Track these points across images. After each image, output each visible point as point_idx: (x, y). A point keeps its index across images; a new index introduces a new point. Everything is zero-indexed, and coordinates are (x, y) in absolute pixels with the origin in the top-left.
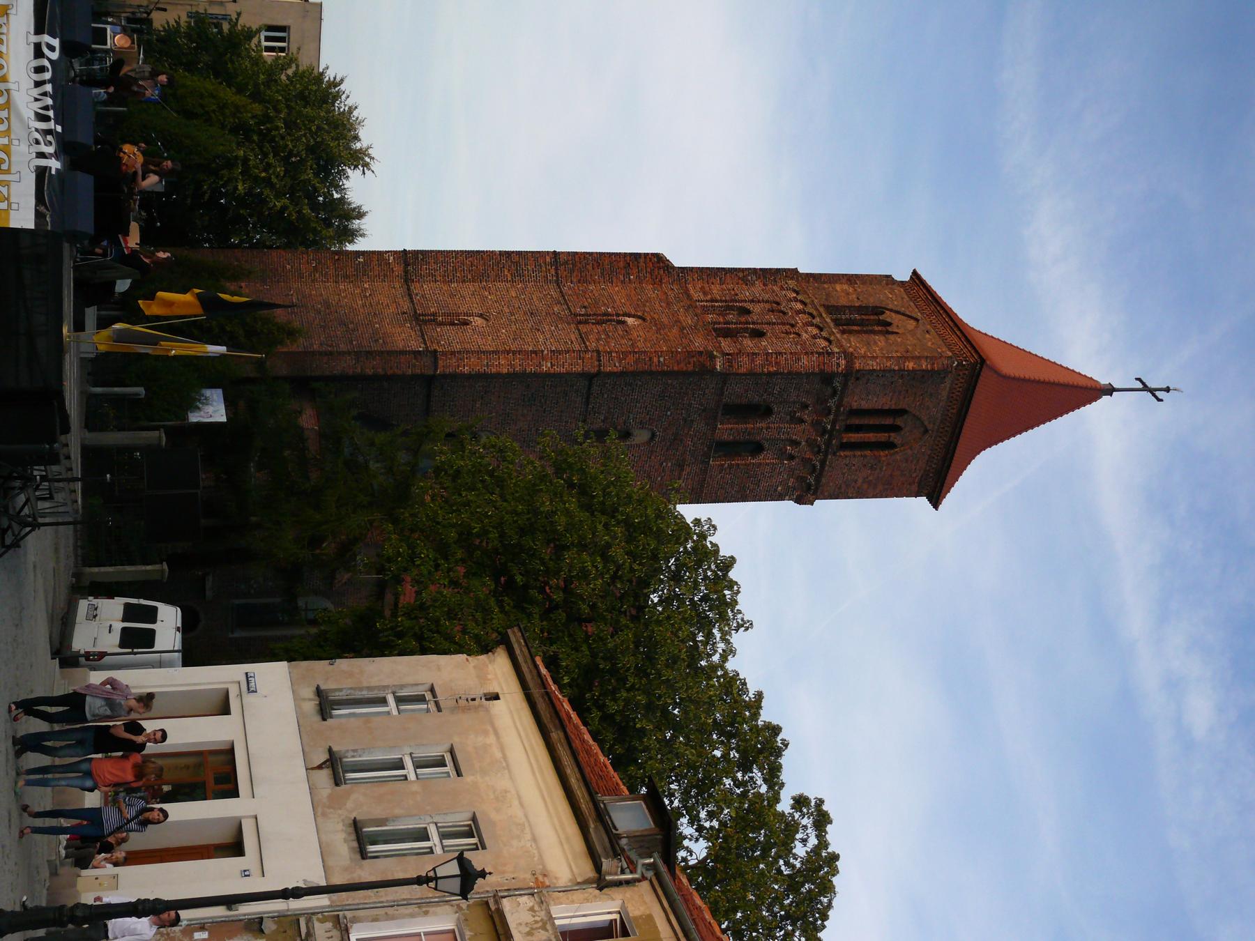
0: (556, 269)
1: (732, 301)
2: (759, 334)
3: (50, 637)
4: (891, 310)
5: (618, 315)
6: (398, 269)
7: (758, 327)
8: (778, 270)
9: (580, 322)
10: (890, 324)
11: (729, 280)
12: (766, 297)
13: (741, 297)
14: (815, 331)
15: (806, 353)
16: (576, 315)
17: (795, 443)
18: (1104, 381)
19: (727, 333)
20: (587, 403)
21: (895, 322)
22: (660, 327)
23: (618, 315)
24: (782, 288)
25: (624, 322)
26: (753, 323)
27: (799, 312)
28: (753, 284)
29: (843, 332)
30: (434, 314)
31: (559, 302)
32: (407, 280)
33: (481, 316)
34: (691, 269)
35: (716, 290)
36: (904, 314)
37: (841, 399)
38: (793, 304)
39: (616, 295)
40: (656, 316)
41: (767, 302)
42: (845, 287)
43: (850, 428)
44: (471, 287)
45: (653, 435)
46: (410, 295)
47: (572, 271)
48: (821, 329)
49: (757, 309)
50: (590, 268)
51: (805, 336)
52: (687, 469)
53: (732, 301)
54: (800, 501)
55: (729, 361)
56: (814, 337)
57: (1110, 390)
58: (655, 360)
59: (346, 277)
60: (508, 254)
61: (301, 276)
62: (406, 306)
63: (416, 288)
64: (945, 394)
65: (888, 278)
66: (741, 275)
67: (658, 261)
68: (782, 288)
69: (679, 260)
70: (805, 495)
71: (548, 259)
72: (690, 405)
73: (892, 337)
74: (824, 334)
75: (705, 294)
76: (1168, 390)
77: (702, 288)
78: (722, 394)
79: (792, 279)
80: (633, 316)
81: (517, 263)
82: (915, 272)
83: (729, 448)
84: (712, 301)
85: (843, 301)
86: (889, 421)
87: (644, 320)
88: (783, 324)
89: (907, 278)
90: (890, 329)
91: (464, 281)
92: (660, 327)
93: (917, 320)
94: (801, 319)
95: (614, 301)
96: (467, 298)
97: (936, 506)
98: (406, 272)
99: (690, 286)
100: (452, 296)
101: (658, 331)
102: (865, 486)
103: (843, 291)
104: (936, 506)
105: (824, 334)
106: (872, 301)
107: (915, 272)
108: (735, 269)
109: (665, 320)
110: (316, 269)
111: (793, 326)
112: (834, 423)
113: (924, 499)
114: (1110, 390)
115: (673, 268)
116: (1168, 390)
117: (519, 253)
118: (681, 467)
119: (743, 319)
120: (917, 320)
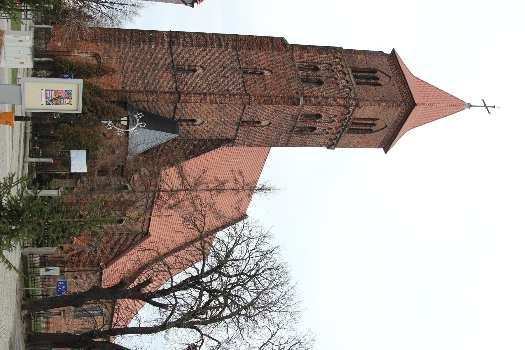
0: (236, 43)
1: (312, 63)
2: (320, 83)
3: (48, 77)
4: (380, 71)
5: (261, 69)
6: (167, 40)
7: (321, 78)
8: (334, 47)
9: (244, 73)
10: (378, 79)
11: (311, 51)
12: (327, 61)
13: (315, 61)
14: (345, 83)
15: (339, 98)
16: (243, 68)
17: (330, 129)
18: (467, 102)
19: (306, 81)
20: (243, 111)
21: (381, 78)
22: (279, 78)
23: (261, 69)
24: (334, 57)
25: (262, 74)
26: (319, 77)
27: (340, 71)
28: (322, 53)
29: (357, 83)
30: (181, 65)
31: (236, 61)
32: (171, 44)
33: (202, 67)
34: (296, 45)
35: (305, 56)
36: (385, 74)
37: (351, 115)
38: (338, 66)
39: (261, 58)
40: (277, 71)
41: (327, 64)
42: (362, 56)
43: (354, 124)
44: (199, 50)
45: (270, 124)
46: (171, 54)
47: (243, 44)
48: (348, 82)
49: (321, 67)
50: (251, 42)
51: (340, 85)
52: (283, 135)
53: (312, 63)
54: (329, 148)
55: (306, 100)
56: (344, 86)
57: (470, 106)
58: (274, 100)
59: (144, 42)
60: (216, 35)
61: (125, 41)
62: (169, 60)
63: (174, 49)
65: (382, 53)
66: (317, 49)
67: (281, 41)
68: (334, 57)
69: (291, 41)
70: (331, 146)
71: (233, 38)
72: (287, 114)
73: (378, 87)
74: (349, 85)
75: (300, 58)
76: (494, 107)
77: (300, 54)
78: (301, 110)
79: (339, 52)
80: (268, 70)
81: (220, 39)
82: (393, 51)
83: (302, 130)
84: (303, 62)
85: (359, 65)
86: (371, 122)
87: (272, 73)
88: (332, 77)
89: (390, 53)
90: (378, 82)
91: (196, 47)
92: (279, 78)
93: (390, 78)
94: (340, 75)
95: (260, 61)
96: (196, 57)
97: (386, 152)
98: (170, 41)
99: (294, 53)
100: (190, 54)
101: (278, 79)
102: (357, 144)
104: (386, 152)
105: (349, 85)
106: (372, 66)
107: (393, 51)
108: (315, 46)
109: (281, 73)
110: (131, 38)
111: (336, 79)
112: (347, 123)
113: (390, 53)
114: (470, 106)
115: (288, 44)
117: (221, 35)
118: (280, 134)
119: (315, 74)
120: (390, 78)
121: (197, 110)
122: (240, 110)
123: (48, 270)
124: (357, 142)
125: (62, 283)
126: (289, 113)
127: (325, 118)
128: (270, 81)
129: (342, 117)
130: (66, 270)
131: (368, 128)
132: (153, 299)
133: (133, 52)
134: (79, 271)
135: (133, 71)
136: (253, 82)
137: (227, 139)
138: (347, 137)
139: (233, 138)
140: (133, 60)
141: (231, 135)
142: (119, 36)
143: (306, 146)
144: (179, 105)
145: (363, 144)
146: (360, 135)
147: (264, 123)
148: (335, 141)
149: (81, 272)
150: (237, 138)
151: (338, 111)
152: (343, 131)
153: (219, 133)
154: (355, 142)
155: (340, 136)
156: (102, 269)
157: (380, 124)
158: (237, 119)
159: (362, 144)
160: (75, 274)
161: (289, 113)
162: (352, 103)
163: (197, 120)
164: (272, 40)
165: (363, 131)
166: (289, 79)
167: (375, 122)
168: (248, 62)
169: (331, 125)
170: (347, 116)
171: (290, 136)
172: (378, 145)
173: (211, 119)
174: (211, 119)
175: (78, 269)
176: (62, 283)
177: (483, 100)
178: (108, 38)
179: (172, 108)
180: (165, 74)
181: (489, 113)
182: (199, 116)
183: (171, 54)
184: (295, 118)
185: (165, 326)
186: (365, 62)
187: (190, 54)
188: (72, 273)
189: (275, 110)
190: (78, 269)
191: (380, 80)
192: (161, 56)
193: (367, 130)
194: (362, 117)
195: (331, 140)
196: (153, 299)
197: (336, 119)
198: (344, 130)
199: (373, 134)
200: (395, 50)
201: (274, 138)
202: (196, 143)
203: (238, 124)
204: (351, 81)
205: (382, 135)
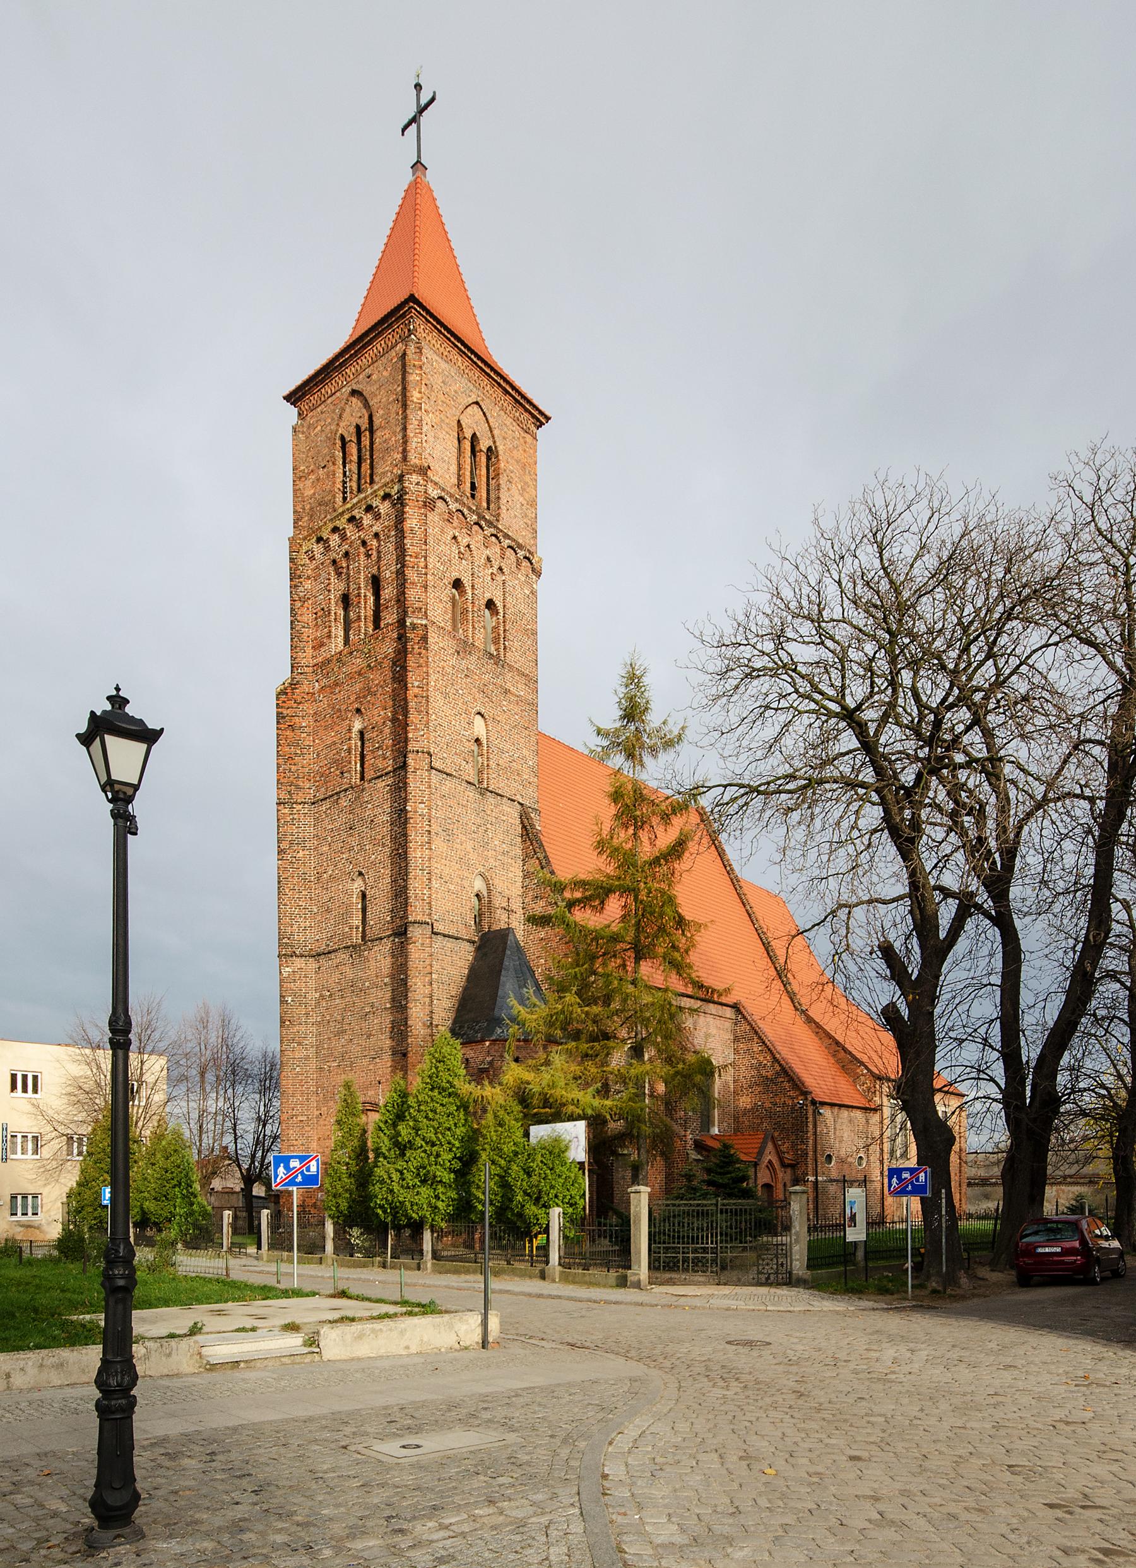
18: (408, 177)
40: (353, 698)
46: (329, 953)
47: (298, 787)
50: (293, 768)
52: (509, 686)
62: (342, 956)
64: (444, 365)
76: (418, 87)
82: (287, 398)
86: (467, 445)
89: (294, 411)
95: (334, 743)
100: (328, 911)
102: (527, 496)
103: (313, 485)
107: (287, 398)
108: (292, 610)
109: (357, 687)
110: (299, 1044)
116: (418, 87)
121: (452, 887)
122: (449, 783)
123: (853, 1217)
124: (522, 495)
125: (895, 1180)
126: (453, 662)
127: (460, 569)
128: (376, 712)
129: (456, 522)
130: (811, 1178)
131: (484, 459)
132: (942, 935)
133: (329, 1039)
134: (815, 1151)
135: (368, 1037)
136: (380, 752)
137: (524, 827)
138: (511, 520)
139: (519, 807)
140: (346, 1037)
141: (512, 814)
142: (298, 1069)
143: (535, 633)
144: (439, 927)
145: (527, 478)
146: (503, 480)
147: (479, 728)
148: (521, 553)
149: (819, 1147)
150: (519, 798)
151: (442, 531)
152: (495, 527)
153: (507, 840)
154: (521, 499)
155: (506, 536)
156: (814, 1102)
157: (473, 422)
158: (471, 794)
159: (526, 483)
160: (821, 1159)
161: (453, 661)
162: (417, 484)
163: (476, 890)
164: (284, 717)
165: (493, 475)
166: (369, 666)
167: (468, 435)
168: (338, 772)
169: (480, 554)
170: (454, 506)
171: (510, 666)
172: (528, 438)
173: (473, 856)
174: (473, 856)
175: (811, 1153)
176: (895, 1180)
177: (404, 130)
178: (302, 1095)
179: (449, 944)
180: (372, 963)
181: (433, 100)
182: (466, 883)
183: (329, 953)
184: (465, 648)
185: (1003, 921)
186: (321, 471)
187: (328, 911)
188: (819, 1166)
189: (446, 695)
190: (811, 1153)
191: (360, 422)
192: (336, 977)
193: (488, 459)
194: (454, 468)
195: (518, 564)
196: (942, 935)
197: (464, 541)
198: (490, 524)
199: (501, 448)
200: (286, 392)
201: (517, 709)
202: (531, 893)
203: (484, 791)
204: (365, 498)
205: (504, 427)
